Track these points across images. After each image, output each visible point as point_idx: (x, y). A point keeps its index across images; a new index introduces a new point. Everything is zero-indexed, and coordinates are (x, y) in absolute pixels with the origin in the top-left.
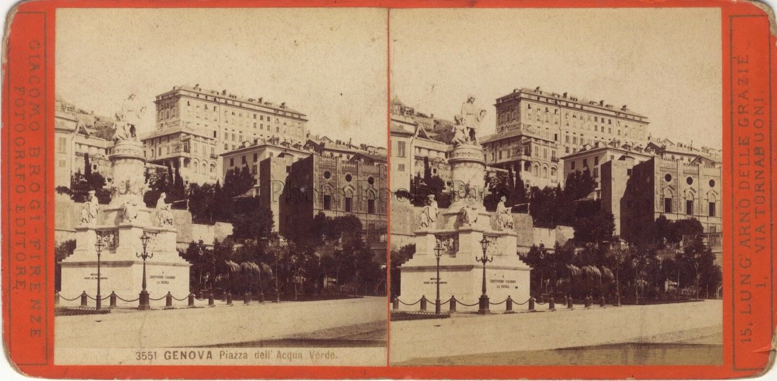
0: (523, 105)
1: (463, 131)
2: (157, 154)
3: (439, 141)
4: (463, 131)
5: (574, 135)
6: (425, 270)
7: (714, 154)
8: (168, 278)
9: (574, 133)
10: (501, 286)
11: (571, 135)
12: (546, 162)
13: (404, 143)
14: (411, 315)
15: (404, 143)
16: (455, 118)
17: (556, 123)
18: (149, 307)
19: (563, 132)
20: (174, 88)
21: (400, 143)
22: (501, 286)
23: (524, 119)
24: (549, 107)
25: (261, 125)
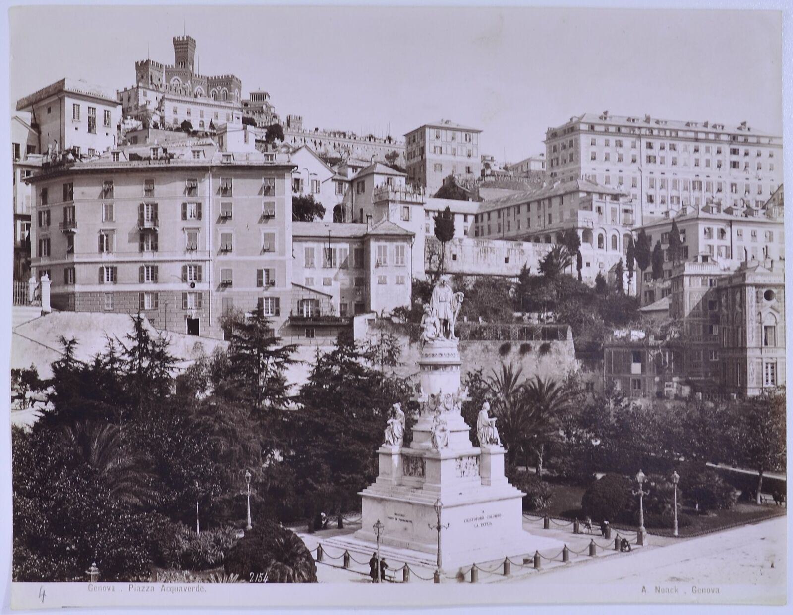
0: (584, 140)
1: (434, 324)
2: (547, 222)
3: (274, 261)
4: (434, 324)
5: (675, 177)
6: (26, 102)
7: (722, 212)
8: (490, 517)
9: (663, 174)
10: (480, 525)
11: (657, 176)
12: (615, 227)
13: (313, 249)
14: (81, 95)
15: (313, 249)
16: (293, 284)
17: (634, 161)
18: (343, 204)
19: (646, 174)
20: (571, 119)
21: (307, 249)
22: (480, 525)
23: (586, 167)
24: (597, 137)
25: (663, 158)
